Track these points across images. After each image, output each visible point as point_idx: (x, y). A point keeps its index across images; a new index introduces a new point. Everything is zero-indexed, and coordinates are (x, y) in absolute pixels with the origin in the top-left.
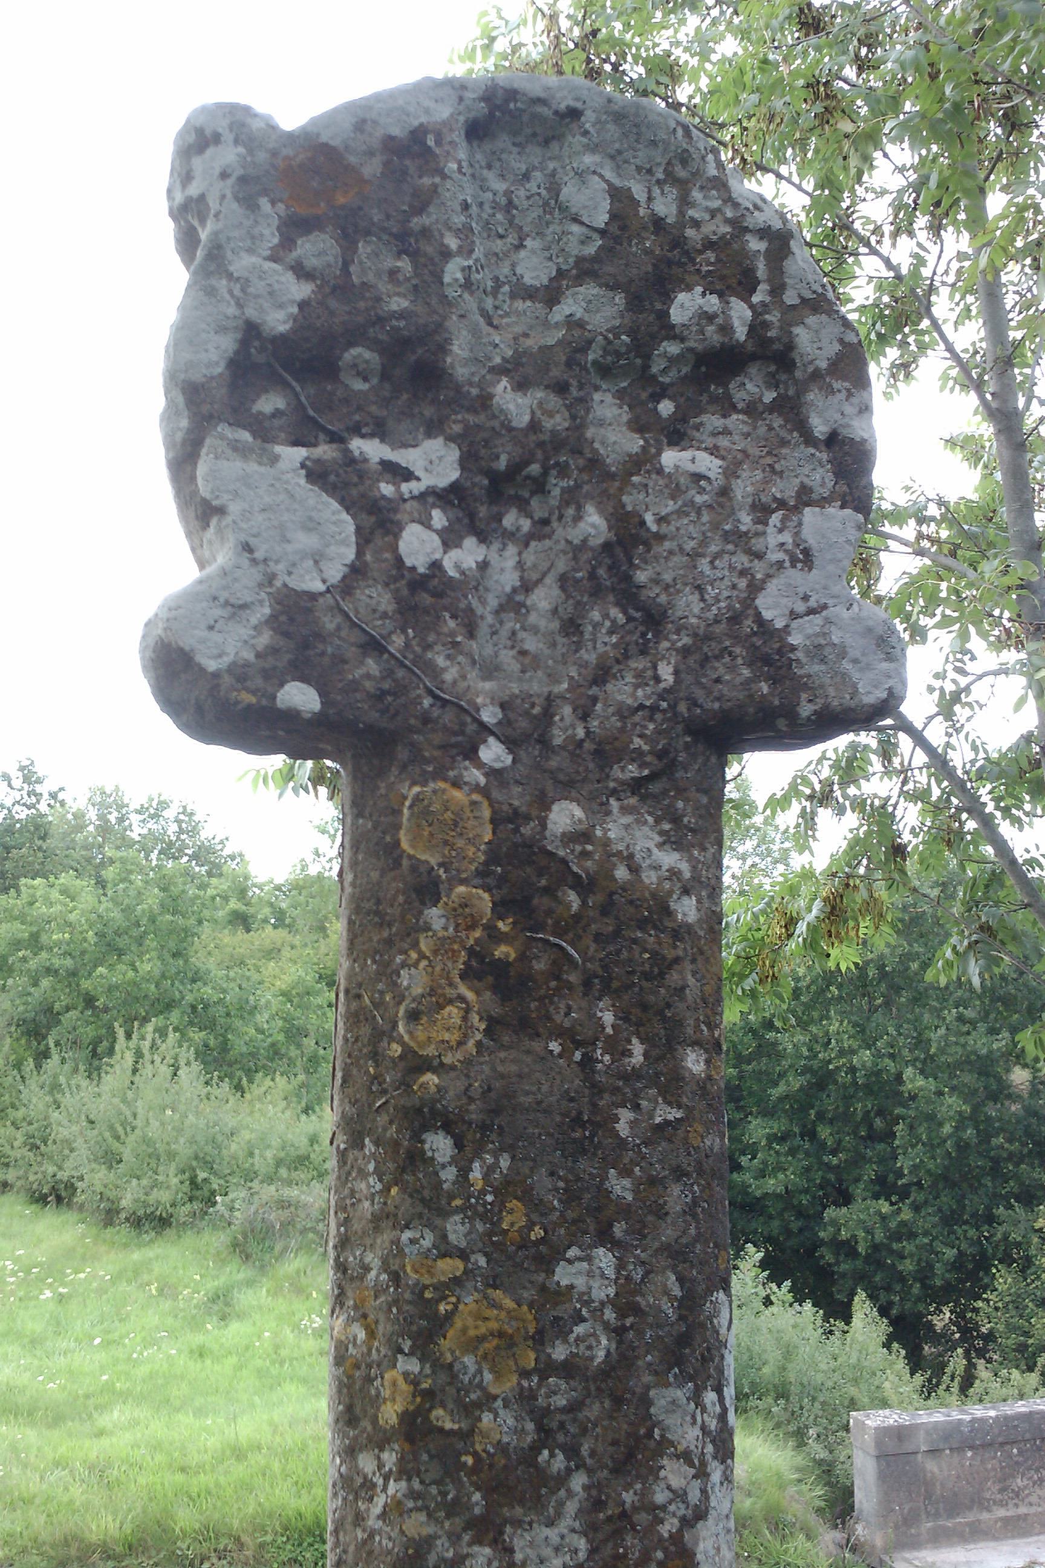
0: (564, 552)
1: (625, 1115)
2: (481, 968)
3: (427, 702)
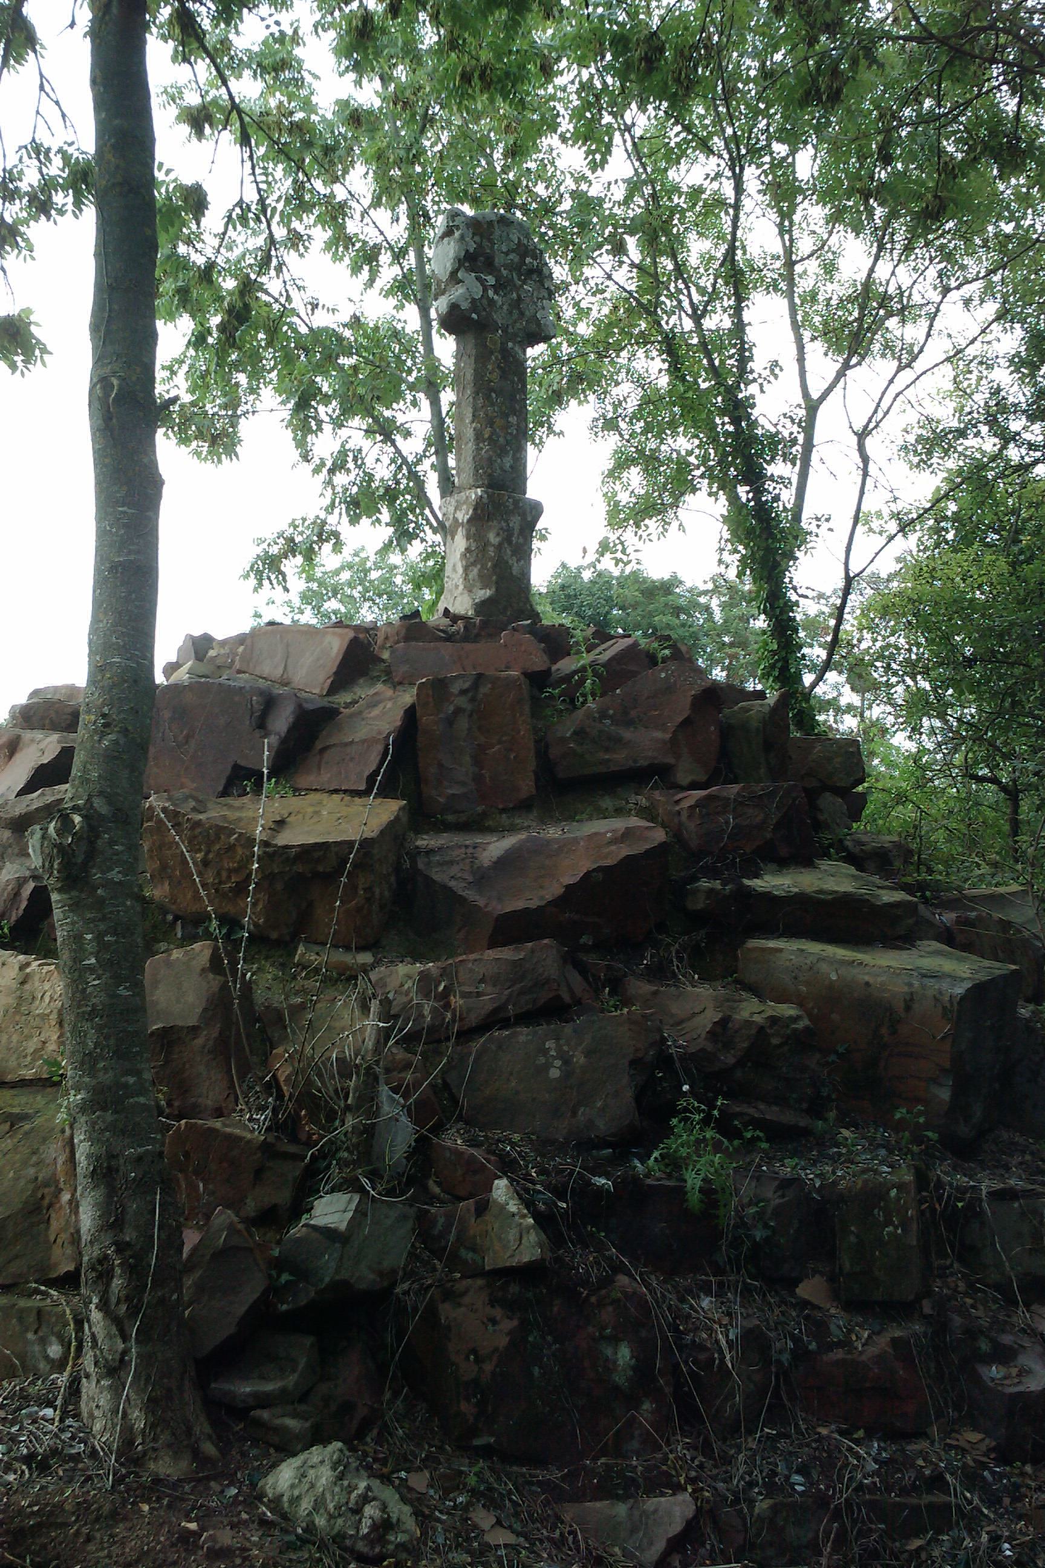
2: (499, 367)
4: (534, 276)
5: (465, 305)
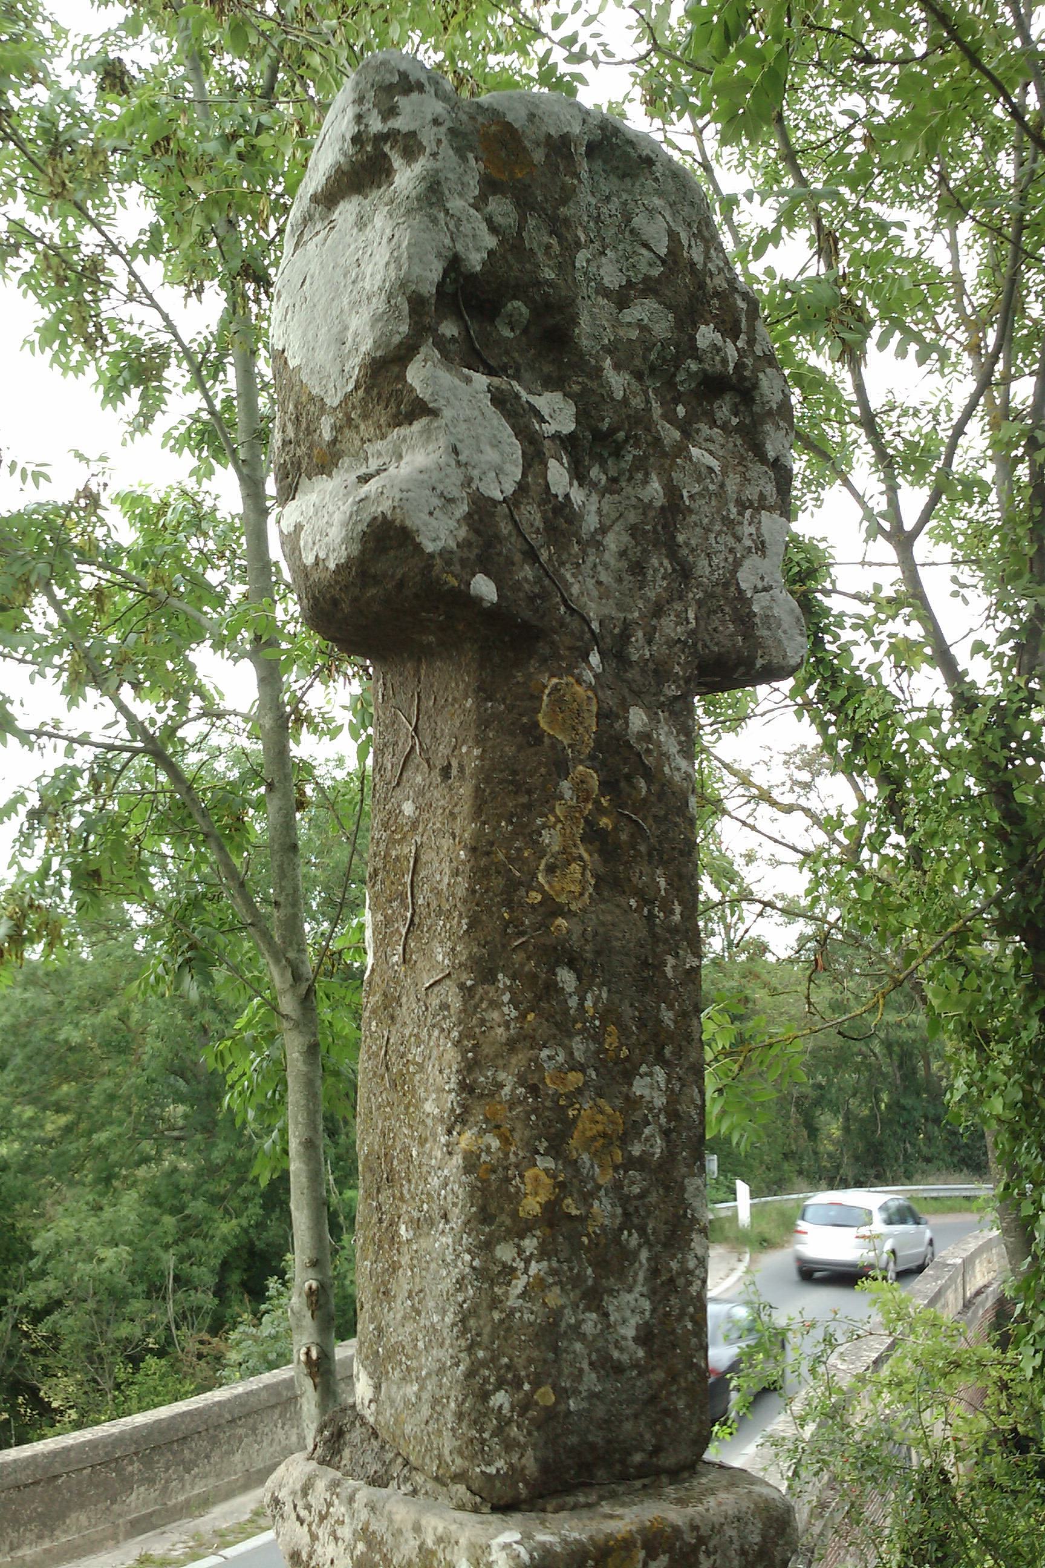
0: (635, 507)
1: (671, 961)
2: (594, 835)
3: (562, 609)
4: (723, 410)
5: (440, 533)
